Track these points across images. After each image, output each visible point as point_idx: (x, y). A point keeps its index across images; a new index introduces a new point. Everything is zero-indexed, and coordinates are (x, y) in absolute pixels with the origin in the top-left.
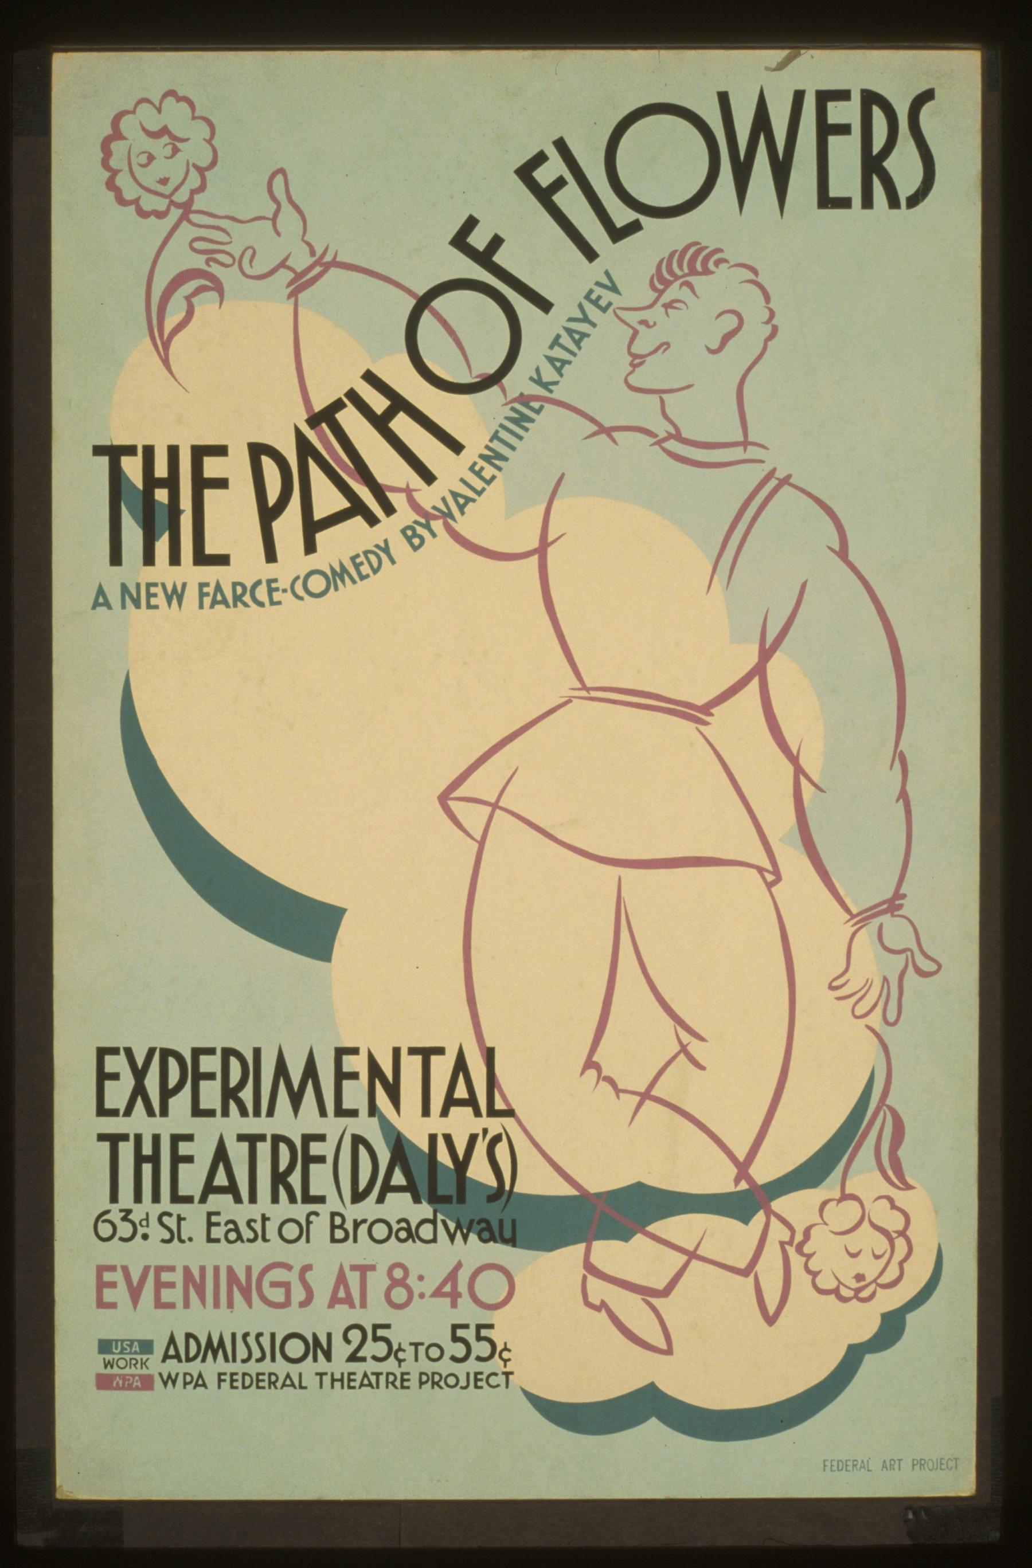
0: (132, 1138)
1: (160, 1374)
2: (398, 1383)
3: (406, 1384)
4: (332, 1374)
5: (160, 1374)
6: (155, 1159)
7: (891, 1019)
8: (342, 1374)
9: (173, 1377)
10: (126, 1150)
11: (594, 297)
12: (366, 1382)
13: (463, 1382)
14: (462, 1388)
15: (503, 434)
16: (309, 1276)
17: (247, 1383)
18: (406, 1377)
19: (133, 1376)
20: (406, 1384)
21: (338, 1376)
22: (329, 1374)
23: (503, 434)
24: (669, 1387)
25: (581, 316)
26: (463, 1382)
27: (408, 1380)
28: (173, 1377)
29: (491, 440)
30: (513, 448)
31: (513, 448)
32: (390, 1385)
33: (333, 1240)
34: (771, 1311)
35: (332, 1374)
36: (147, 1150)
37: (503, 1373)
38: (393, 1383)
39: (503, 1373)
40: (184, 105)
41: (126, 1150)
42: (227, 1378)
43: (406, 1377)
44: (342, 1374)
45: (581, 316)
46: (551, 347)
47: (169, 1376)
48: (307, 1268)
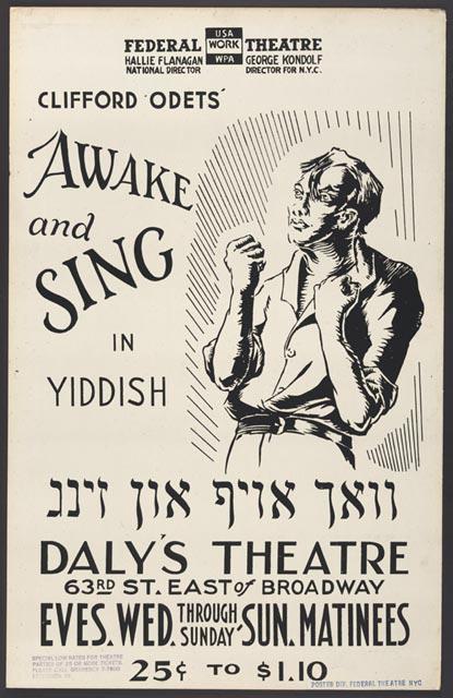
1: (338, 582)
2: (124, 103)
3: (189, 103)
4: (250, 545)
5: (338, 582)
7: (213, 590)
8: (268, 545)
9: (349, 585)
12: (363, 587)
14: (394, 606)
15: (345, 612)
19: (229, 55)
20: (189, 103)
21: (259, 548)
22: (245, 546)
23: (345, 612)
24: (244, 287)
27: (191, 99)
28: (349, 585)
29: (334, 606)
32: (369, 567)
33: (264, 593)
35: (250, 545)
38: (119, 103)
42: (81, 97)
44: (268, 545)
45: (78, 565)
46: (334, 606)
47: (345, 583)
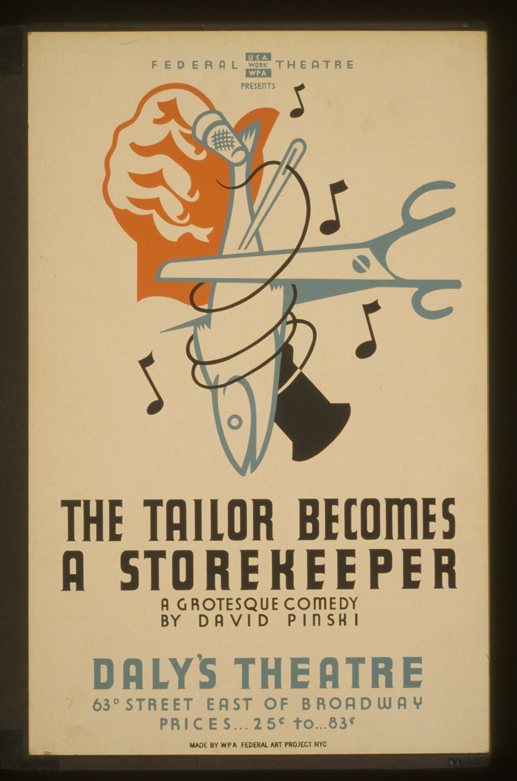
0: (82, 503)
6: (98, 520)
10: (79, 512)
11: (230, 602)
13: (298, 745)
16: (452, 509)
17: (344, 605)
18: (213, 722)
25: (354, 600)
26: (298, 745)
27: (213, 704)
30: (267, 599)
31: (267, 599)
34: (236, 621)
36: (93, 513)
37: (148, 554)
39: (148, 554)
40: (447, 522)
41: (79, 512)
43: (213, 722)
45: (354, 600)
48: (448, 502)
